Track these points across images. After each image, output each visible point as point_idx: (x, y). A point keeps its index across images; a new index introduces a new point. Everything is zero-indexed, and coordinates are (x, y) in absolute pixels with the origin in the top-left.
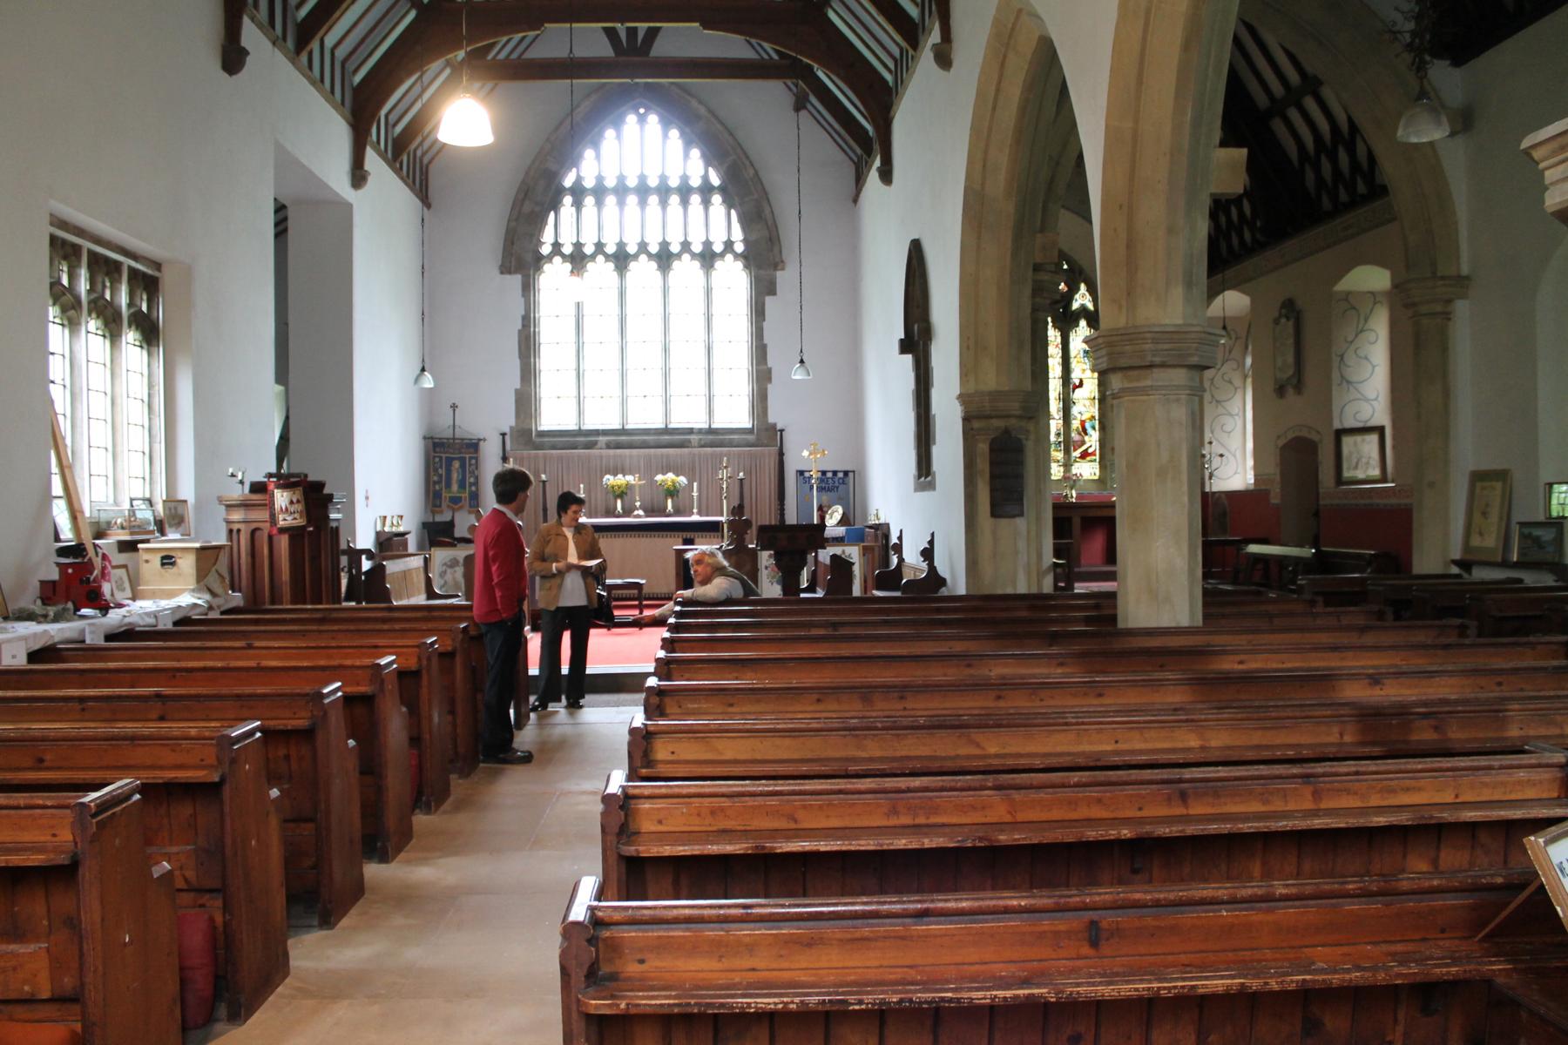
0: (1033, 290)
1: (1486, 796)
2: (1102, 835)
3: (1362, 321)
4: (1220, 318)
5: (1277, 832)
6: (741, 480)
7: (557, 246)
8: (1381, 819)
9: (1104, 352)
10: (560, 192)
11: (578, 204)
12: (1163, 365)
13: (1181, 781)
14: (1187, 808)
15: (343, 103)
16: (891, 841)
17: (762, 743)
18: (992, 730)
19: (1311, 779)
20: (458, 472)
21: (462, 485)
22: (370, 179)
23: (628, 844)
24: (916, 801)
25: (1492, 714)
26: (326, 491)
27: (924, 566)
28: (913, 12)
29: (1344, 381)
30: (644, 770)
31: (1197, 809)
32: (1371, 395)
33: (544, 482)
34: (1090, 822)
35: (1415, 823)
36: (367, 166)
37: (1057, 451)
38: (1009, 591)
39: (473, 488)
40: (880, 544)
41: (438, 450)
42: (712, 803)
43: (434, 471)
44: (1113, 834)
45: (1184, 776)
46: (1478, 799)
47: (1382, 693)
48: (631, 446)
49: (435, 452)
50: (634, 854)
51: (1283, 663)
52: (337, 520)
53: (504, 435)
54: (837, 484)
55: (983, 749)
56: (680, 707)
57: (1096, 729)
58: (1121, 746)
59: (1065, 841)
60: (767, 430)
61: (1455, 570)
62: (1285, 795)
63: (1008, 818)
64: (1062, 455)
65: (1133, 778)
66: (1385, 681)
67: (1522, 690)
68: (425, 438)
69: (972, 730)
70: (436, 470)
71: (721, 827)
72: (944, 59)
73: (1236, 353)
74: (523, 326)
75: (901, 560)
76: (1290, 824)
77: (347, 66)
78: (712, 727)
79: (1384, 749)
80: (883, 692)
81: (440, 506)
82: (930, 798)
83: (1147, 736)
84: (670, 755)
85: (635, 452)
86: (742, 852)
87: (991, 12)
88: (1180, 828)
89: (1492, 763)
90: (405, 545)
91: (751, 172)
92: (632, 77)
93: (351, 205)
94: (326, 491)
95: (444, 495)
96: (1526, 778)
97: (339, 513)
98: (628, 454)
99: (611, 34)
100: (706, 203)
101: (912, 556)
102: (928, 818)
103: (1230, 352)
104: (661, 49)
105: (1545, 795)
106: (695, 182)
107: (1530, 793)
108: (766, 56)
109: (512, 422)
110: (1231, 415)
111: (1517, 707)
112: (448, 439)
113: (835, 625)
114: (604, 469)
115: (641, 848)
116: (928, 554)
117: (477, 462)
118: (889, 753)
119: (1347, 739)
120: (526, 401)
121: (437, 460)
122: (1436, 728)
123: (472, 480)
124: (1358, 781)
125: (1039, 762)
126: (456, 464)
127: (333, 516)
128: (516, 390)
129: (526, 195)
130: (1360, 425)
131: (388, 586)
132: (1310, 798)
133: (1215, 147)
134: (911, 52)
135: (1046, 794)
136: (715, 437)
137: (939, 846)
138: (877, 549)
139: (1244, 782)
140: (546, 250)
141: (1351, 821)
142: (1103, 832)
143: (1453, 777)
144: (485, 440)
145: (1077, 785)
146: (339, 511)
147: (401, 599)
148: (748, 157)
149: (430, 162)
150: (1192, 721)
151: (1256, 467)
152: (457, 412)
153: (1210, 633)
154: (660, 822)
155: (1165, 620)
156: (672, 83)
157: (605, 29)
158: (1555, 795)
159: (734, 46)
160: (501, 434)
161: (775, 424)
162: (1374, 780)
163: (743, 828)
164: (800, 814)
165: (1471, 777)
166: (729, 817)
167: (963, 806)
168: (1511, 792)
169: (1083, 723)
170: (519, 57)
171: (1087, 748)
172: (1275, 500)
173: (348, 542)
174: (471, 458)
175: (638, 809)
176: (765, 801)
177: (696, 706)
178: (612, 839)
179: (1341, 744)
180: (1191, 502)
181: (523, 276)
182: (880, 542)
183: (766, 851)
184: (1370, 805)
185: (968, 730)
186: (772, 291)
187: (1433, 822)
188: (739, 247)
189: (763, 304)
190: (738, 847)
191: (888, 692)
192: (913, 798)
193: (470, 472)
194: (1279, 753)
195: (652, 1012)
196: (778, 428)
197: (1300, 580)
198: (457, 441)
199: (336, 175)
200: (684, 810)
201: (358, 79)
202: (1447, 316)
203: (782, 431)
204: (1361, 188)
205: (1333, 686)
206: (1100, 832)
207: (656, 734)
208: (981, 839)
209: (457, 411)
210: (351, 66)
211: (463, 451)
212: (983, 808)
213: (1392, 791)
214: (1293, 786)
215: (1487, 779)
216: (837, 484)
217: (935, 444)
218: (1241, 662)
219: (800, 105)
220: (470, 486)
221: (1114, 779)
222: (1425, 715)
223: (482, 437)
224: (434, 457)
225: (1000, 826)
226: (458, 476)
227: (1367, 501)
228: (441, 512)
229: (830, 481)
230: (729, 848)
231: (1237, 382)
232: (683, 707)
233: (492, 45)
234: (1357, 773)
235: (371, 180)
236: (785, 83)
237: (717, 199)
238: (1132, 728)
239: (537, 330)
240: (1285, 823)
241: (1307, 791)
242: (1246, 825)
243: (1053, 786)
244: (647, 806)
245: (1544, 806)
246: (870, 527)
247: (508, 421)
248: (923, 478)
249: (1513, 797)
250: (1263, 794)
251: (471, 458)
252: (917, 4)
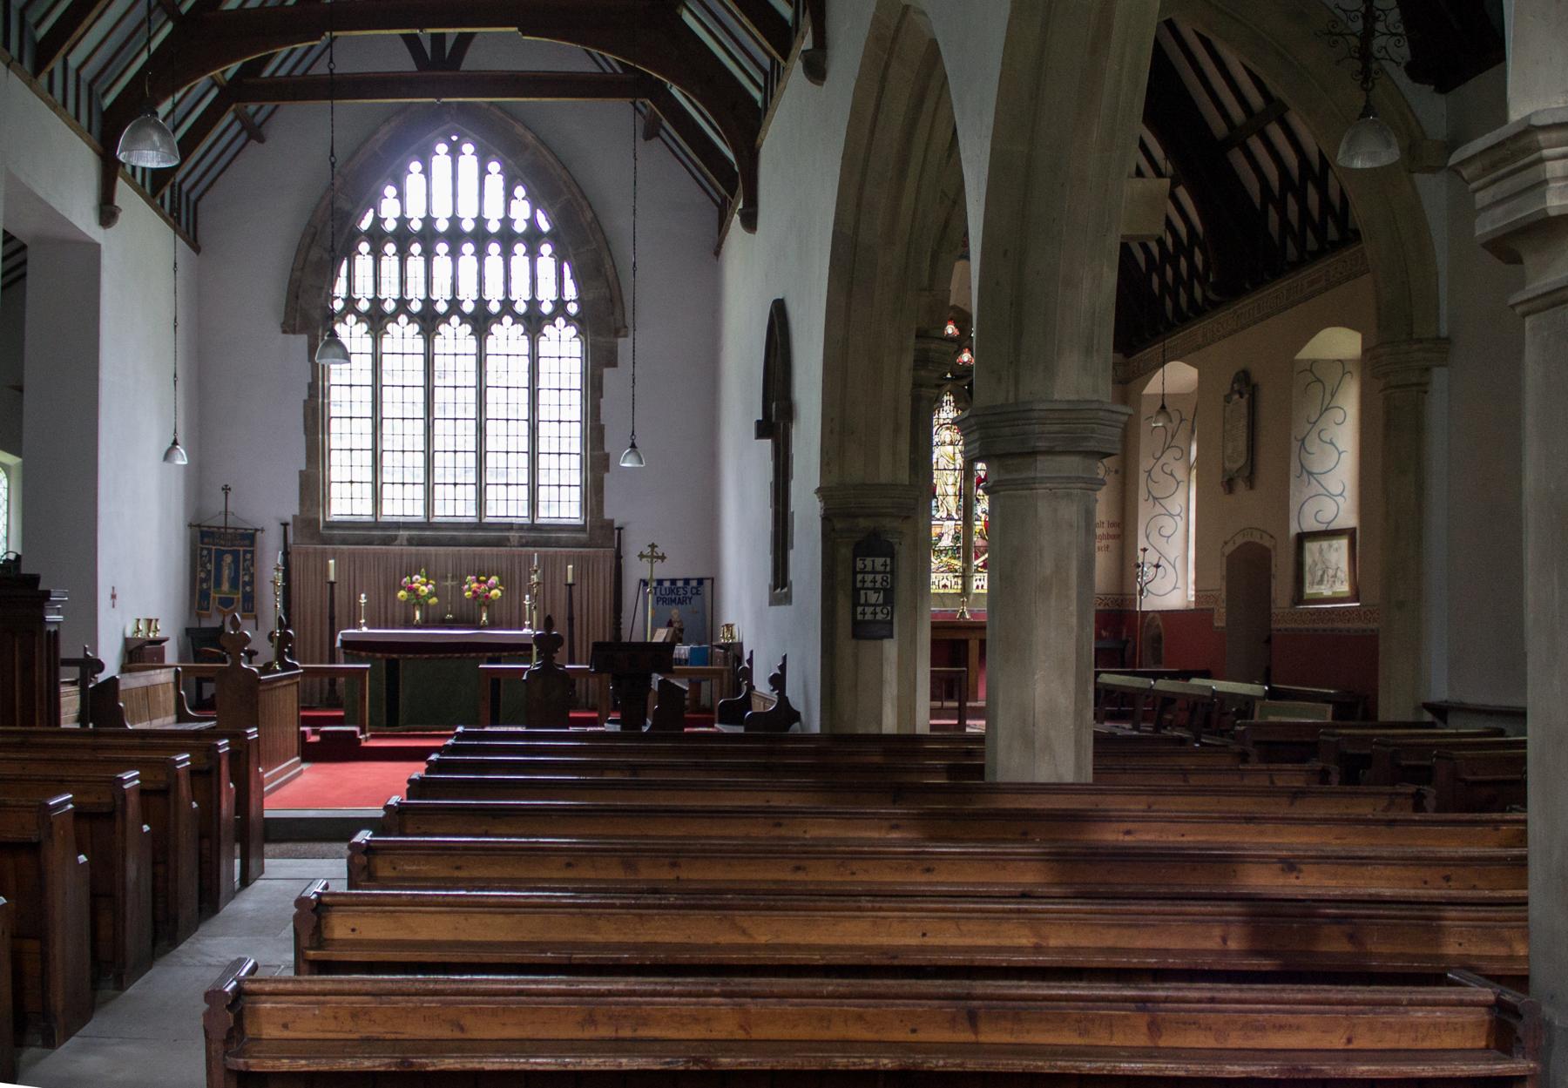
0: (915, 361)
1: (1389, 1041)
2: (854, 1064)
3: (1328, 397)
4: (1156, 395)
5: (1089, 1075)
6: (570, 586)
7: (351, 302)
8: (1236, 1068)
9: (976, 435)
10: (355, 236)
11: (377, 254)
12: (1050, 452)
13: (970, 997)
14: (976, 1033)
15: (90, 130)
16: (578, 1060)
17: (466, 919)
18: (763, 913)
19: (1149, 1005)
20: (230, 568)
21: (234, 583)
22: (121, 215)
23: (238, 1055)
24: (619, 1008)
25: (1424, 922)
26: (42, 587)
27: (774, 696)
28: (787, 12)
29: (1305, 473)
30: (312, 952)
31: (991, 1035)
32: (1335, 488)
33: (332, 584)
34: (846, 1045)
35: (1284, 1077)
36: (119, 200)
37: (955, 558)
38: (873, 730)
39: (248, 589)
40: (730, 667)
41: (206, 540)
42: (353, 1003)
43: (201, 566)
44: (869, 1063)
45: (974, 992)
46: (1380, 1046)
47: (1297, 882)
48: (437, 542)
49: (202, 543)
50: (243, 1068)
51: (1183, 835)
52: (58, 623)
53: (285, 525)
54: (689, 595)
55: (750, 936)
56: (394, 868)
57: (899, 917)
58: (931, 941)
59: (806, 1068)
60: (602, 527)
61: (1428, 717)
62: (1110, 1024)
63: (740, 1035)
64: (960, 564)
65: (907, 989)
66: (1303, 867)
67: (1474, 888)
68: (190, 525)
69: (736, 912)
70: (203, 565)
71: (364, 1033)
72: (816, 70)
73: (1180, 439)
74: (310, 396)
75: (751, 687)
76: (1109, 1066)
77: (94, 88)
78: (404, 898)
79: (1277, 962)
80: (652, 857)
81: (208, 609)
82: (639, 1004)
83: (963, 928)
84: (350, 932)
85: (442, 549)
86: (382, 1069)
87: (869, 10)
88: (958, 1061)
89: (1398, 996)
90: (160, 655)
91: (589, 215)
92: (438, 97)
93: (99, 245)
94: (42, 587)
95: (212, 595)
96: (1444, 1020)
97: (58, 614)
98: (433, 552)
99: (412, 42)
100: (533, 254)
101: (762, 685)
102: (635, 1030)
103: (1173, 437)
104: (472, 61)
105: (1468, 1045)
106: (520, 227)
107: (1449, 1042)
108: (609, 70)
109: (296, 511)
110: (1171, 515)
111: (1454, 914)
112: (219, 528)
113: (634, 769)
114: (404, 569)
115: (251, 1061)
116: (778, 681)
117: (252, 557)
118: (630, 938)
119: (1233, 945)
120: (313, 485)
121: (205, 552)
122: (1351, 938)
123: (247, 578)
124: (1212, 1011)
125: (818, 957)
126: (228, 559)
127: (50, 617)
128: (301, 472)
129: (313, 240)
130: (1323, 527)
131: (121, 704)
132: (1144, 1029)
133: (1130, 176)
134: (783, 63)
135: (791, 1005)
136: (537, 534)
137: (641, 1068)
138: (725, 674)
139: (1055, 1003)
140: (338, 305)
141: (1192, 1067)
142: (856, 1060)
143: (1347, 1013)
144: (262, 530)
145: (830, 996)
146: (59, 612)
147: (140, 721)
148: (585, 197)
149: (199, 198)
150: (1026, 911)
151: (1197, 582)
152: (229, 496)
153: (1102, 792)
154: (285, 1026)
155: (1043, 774)
156: (492, 103)
157: (404, 36)
158: (1483, 1044)
159: (569, 57)
160: (282, 524)
161: (612, 521)
162: (1236, 1011)
163: (393, 1036)
164: (468, 1021)
165: (1370, 1016)
166: (374, 1021)
167: (682, 1017)
168: (1423, 1040)
169: (880, 909)
170: (304, 74)
171: (884, 940)
172: (1220, 622)
173: (85, 649)
174: (245, 552)
175: (258, 1009)
176: (423, 1002)
177: (414, 868)
178: (218, 1047)
179: (1225, 953)
180: (1081, 626)
181: (309, 337)
182: (735, 661)
183: (415, 1069)
184: (1229, 1046)
185: (730, 912)
186: (612, 362)
187: (1309, 1076)
188: (573, 309)
189: (601, 377)
190: (378, 1062)
191: (657, 857)
192: (617, 1004)
193: (244, 570)
194: (1135, 960)
195: (1185, 967)
196: (616, 525)
197: (1239, 725)
198: (229, 531)
199: (82, 214)
200: (317, 1012)
201: (108, 101)
202: (1423, 387)
203: (620, 529)
204: (1333, 233)
205: (1234, 871)
206: (851, 1060)
207: (332, 906)
208: (696, 1060)
209: (230, 495)
210: (99, 88)
211: (237, 543)
212: (709, 1020)
213: (1261, 1028)
214: (1123, 1013)
215: (1391, 1019)
216: (689, 595)
217: (792, 548)
218: (1128, 832)
219: (651, 132)
220: (244, 587)
221: (882, 990)
222: (1338, 919)
223: (259, 527)
224: (202, 549)
225: (727, 1045)
226: (230, 573)
227: (1329, 626)
228: (210, 616)
229: (681, 591)
230: (367, 1064)
231: (1180, 474)
232: (398, 868)
233: (269, 58)
234: (1212, 1000)
235: (122, 217)
236: (634, 104)
237: (546, 249)
238: (944, 918)
239: (326, 401)
240: (1102, 1064)
241: (1142, 1020)
242: (1048, 1063)
243: (800, 995)
244: (268, 1005)
245: (1466, 1061)
246: (720, 647)
247: (290, 508)
248: (779, 590)
249: (1427, 1045)
250: (1081, 1021)
251: (245, 552)
252: (791, 4)
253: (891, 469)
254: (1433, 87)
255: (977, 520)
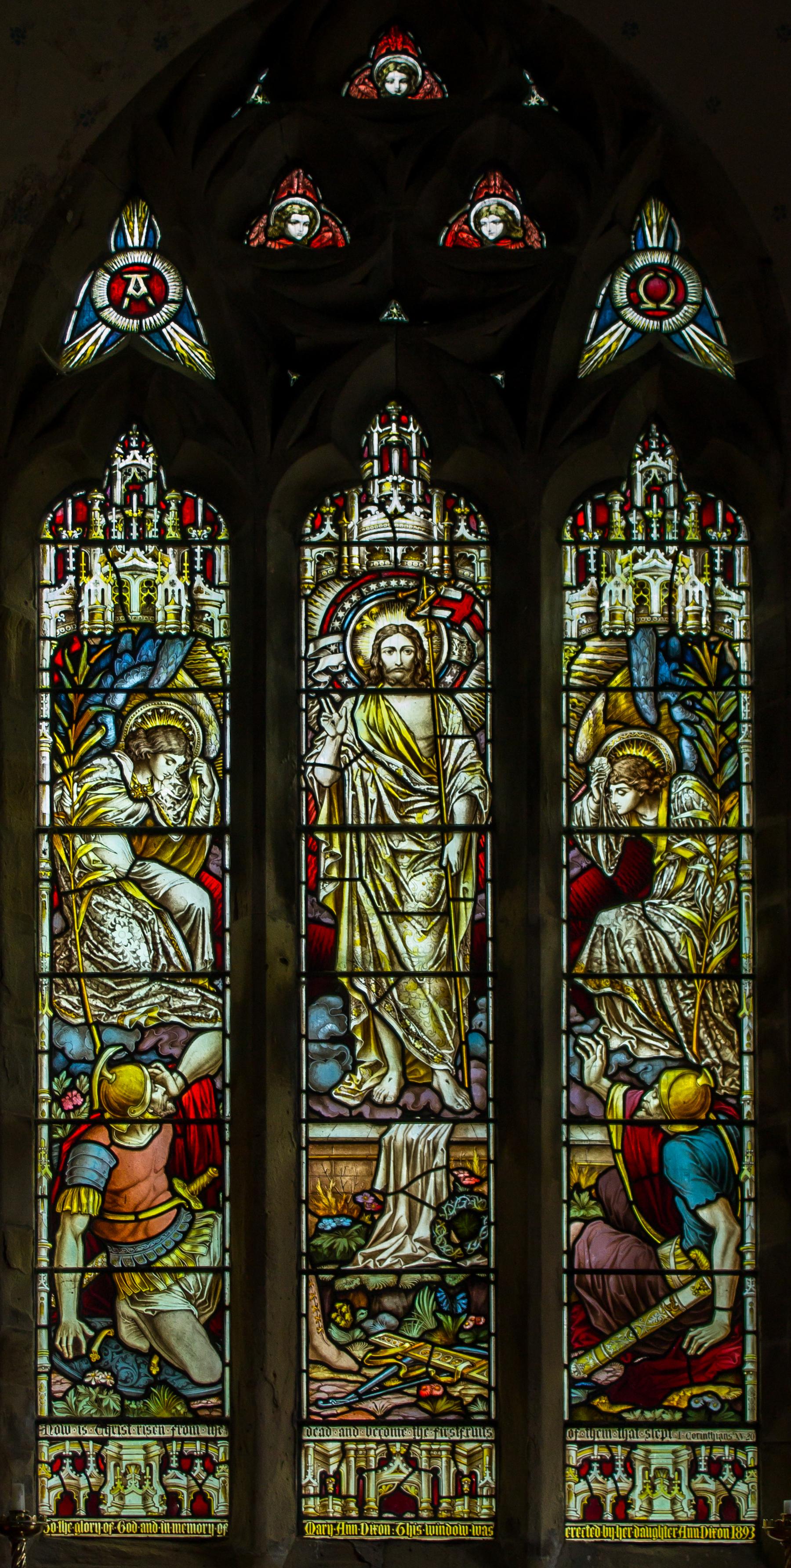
37: (453, 1342)
253: (310, 899)
254: (101, 1507)
255: (585, 1120)
